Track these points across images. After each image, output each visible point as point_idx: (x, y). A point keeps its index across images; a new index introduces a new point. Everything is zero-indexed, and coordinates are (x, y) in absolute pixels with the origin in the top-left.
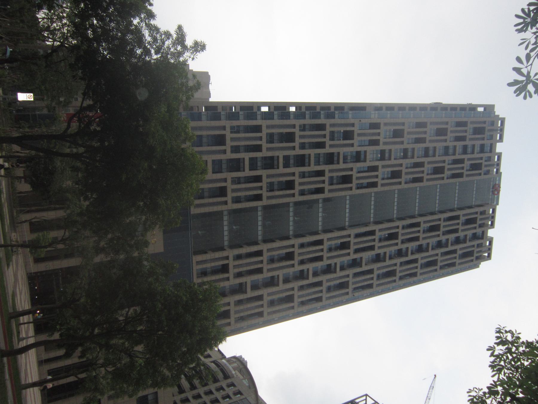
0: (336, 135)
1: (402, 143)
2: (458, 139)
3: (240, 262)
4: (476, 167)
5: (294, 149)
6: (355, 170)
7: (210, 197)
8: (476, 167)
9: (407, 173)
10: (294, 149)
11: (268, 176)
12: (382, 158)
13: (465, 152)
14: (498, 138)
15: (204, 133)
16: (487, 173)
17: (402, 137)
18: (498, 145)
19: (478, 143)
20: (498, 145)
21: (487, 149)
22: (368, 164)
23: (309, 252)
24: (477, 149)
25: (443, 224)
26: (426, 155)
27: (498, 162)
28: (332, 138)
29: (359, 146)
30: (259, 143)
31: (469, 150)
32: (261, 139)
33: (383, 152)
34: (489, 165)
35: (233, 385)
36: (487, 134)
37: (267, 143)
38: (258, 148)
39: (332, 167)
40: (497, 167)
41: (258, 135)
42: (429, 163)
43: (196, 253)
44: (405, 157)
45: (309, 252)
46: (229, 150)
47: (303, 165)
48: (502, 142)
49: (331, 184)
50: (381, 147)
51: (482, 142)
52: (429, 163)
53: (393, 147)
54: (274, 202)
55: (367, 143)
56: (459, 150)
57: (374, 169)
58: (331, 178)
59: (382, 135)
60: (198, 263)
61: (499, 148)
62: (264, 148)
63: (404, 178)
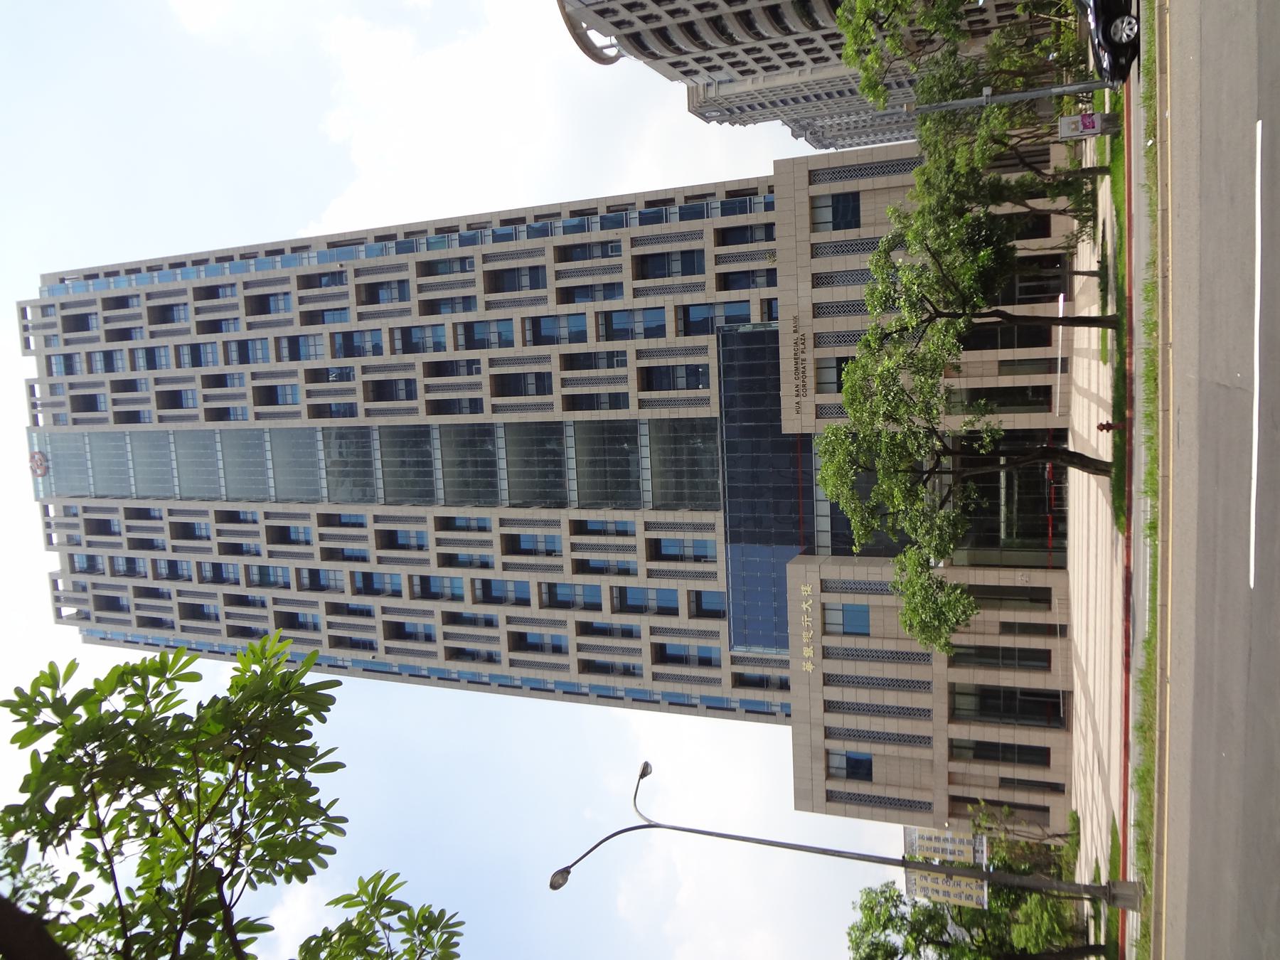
0: (395, 293)
1: (254, 376)
2: (130, 385)
3: (606, 279)
4: (79, 323)
5: (484, 256)
6: (353, 314)
7: (667, 255)
8: (102, 527)
9: (235, 307)
10: (484, 256)
11: (549, 406)
12: (294, 342)
13: (109, 357)
14: (37, 387)
15: (679, 280)
16: (67, 511)
17: (248, 299)
18: (34, 374)
19: (81, 376)
20: (34, 374)
21: (58, 366)
22: (324, 329)
23: (468, 543)
24: (81, 364)
25: (174, 616)
26: (196, 350)
27: (26, 334)
28: (410, 383)
29: (344, 309)
31: (99, 363)
32: (564, 382)
33: (295, 355)
34: (46, 326)
35: (619, 24)
36: (65, 397)
37: (550, 374)
38: (570, 362)
39: (405, 322)
40: (25, 322)
42: (186, 331)
43: (707, 426)
44: (243, 346)
45: (468, 543)
46: (625, 246)
47: (469, 327)
48: (19, 303)
49: (403, 284)
50: (301, 366)
51: (72, 379)
52: (186, 331)
53: (273, 366)
54: (545, 514)
55: (327, 316)
56: (122, 362)
57: (311, 318)
58: (403, 297)
59: (294, 299)
60: (705, 401)
61: (30, 367)
62: (556, 362)
63: (239, 297)
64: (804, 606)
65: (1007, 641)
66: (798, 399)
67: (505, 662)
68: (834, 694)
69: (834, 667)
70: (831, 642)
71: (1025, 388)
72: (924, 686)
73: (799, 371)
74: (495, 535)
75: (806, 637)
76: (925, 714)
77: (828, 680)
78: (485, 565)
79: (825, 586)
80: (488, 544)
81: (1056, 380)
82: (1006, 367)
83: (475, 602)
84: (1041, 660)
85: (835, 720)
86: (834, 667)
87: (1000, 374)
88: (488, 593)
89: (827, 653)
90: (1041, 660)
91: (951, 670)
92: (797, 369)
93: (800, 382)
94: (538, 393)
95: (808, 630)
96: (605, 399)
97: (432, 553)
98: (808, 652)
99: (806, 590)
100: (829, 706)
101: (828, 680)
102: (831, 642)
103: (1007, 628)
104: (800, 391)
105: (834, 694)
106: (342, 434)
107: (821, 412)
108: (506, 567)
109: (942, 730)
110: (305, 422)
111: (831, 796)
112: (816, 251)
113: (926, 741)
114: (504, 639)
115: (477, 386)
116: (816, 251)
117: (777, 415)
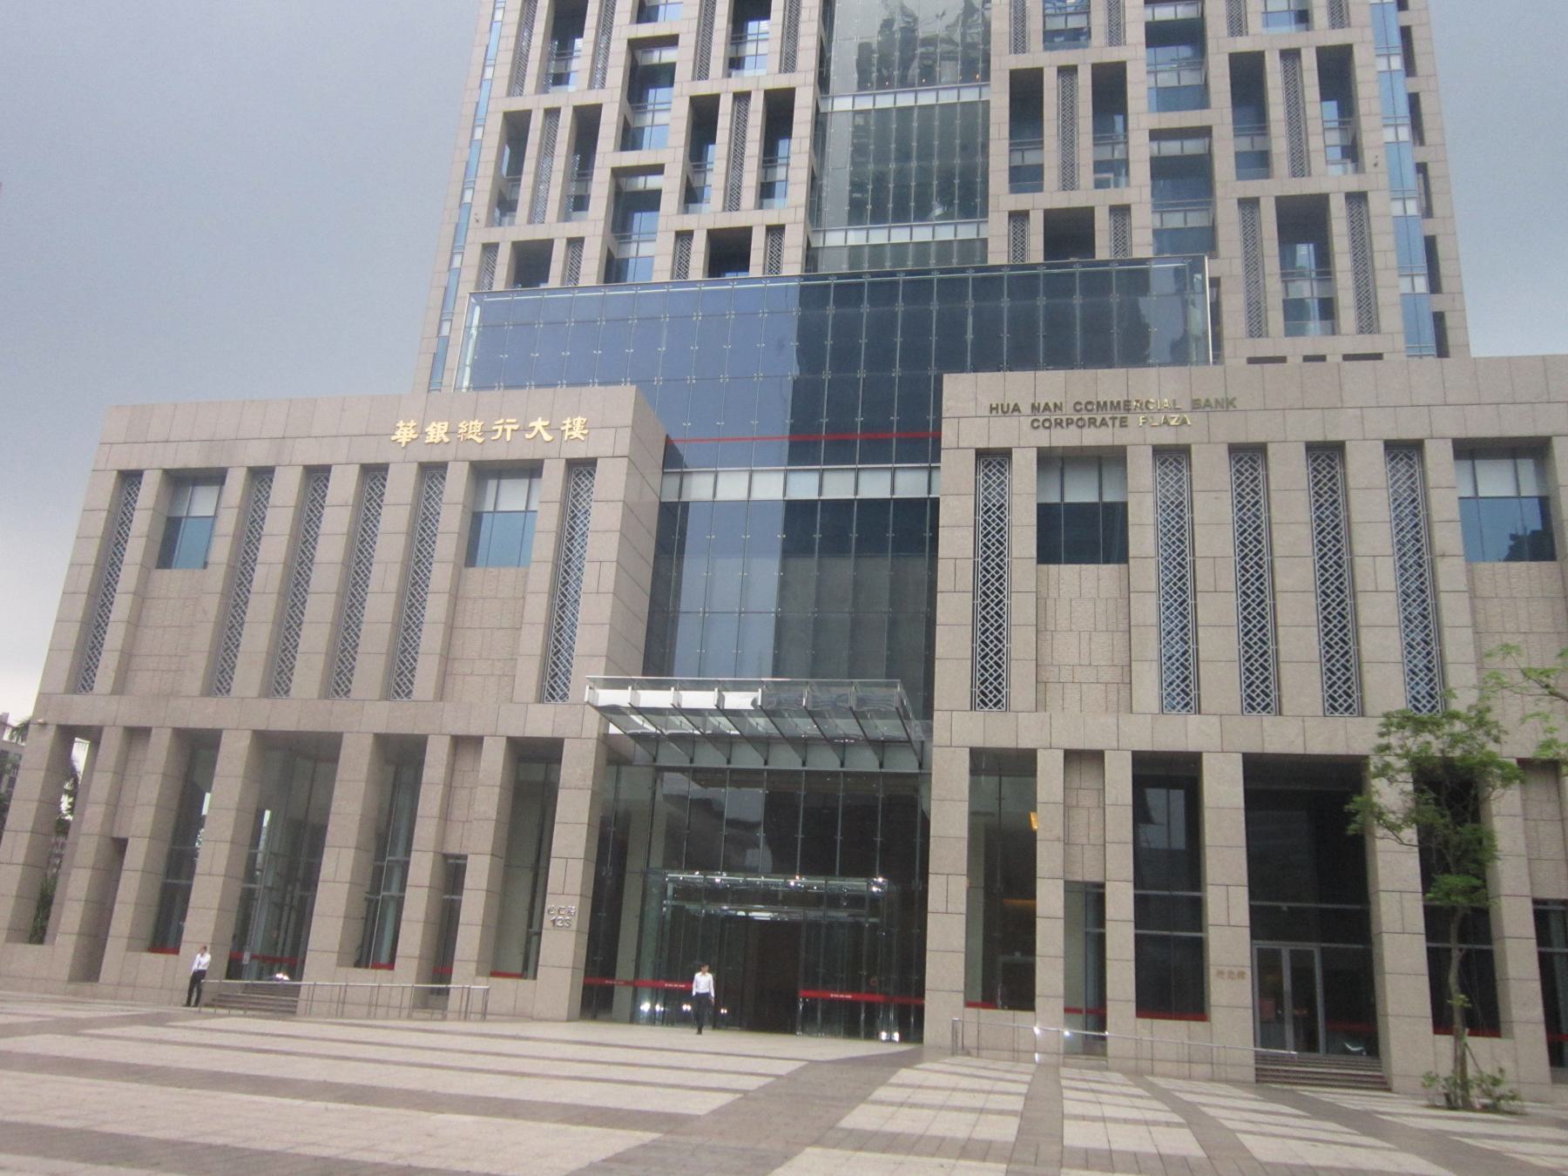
30: (1084, 79)
41: (1051, 82)
64: (539, 424)
65: (422, 869)
66: (1025, 408)
67: (494, 235)
68: (343, 486)
69: (400, 487)
70: (456, 482)
71: (1030, 949)
72: (338, 680)
73: (1091, 413)
74: (750, 216)
75: (472, 429)
76: (278, 681)
77: (374, 474)
78: (692, 195)
79: (580, 468)
80: (732, 200)
81: (1047, 1024)
82: (1088, 901)
83: (619, 173)
84: (371, 946)
85: (1289, 476)
86: (400, 487)
87: (1071, 887)
88: (631, 203)
89: (432, 472)
90: (371, 946)
91: (368, 741)
92: (1102, 406)
93: (1068, 412)
94: (1046, 514)
95: (484, 432)
96: (1031, 158)
97: (718, 84)
98: (437, 431)
99: (575, 427)
100: (317, 475)
101: (374, 474)
102: (456, 482)
103: (452, 872)
104: (1044, 414)
105: (343, 486)
106: (976, 145)
107: (993, 459)
108: (684, 237)
109: (239, 719)
110: (1004, 62)
111: (130, 479)
112: (1404, 451)
113: (219, 681)
114: (538, 233)
115: (1068, 181)
116: (1404, 451)
117: (987, 360)
